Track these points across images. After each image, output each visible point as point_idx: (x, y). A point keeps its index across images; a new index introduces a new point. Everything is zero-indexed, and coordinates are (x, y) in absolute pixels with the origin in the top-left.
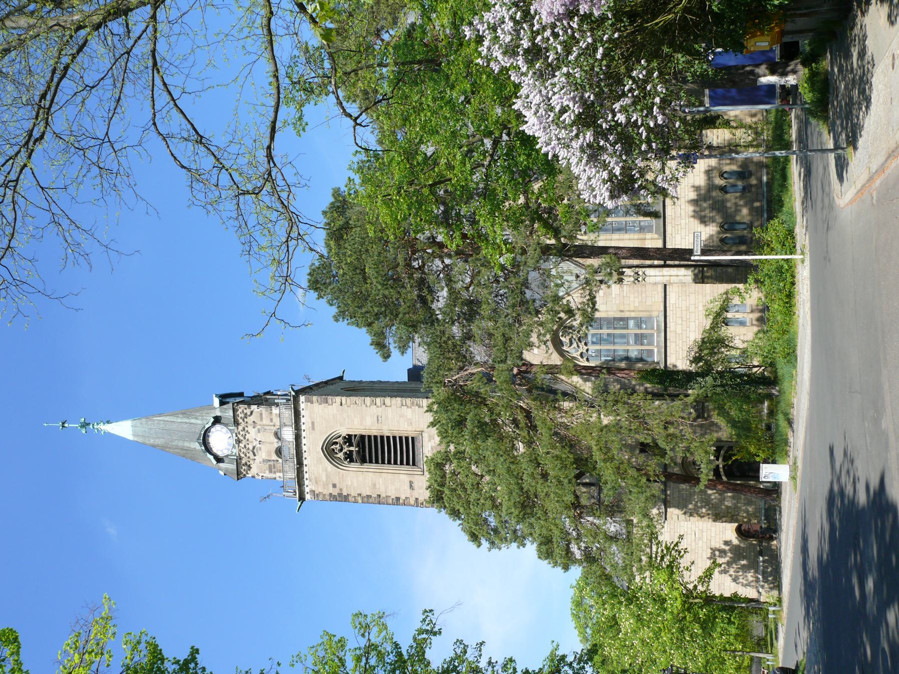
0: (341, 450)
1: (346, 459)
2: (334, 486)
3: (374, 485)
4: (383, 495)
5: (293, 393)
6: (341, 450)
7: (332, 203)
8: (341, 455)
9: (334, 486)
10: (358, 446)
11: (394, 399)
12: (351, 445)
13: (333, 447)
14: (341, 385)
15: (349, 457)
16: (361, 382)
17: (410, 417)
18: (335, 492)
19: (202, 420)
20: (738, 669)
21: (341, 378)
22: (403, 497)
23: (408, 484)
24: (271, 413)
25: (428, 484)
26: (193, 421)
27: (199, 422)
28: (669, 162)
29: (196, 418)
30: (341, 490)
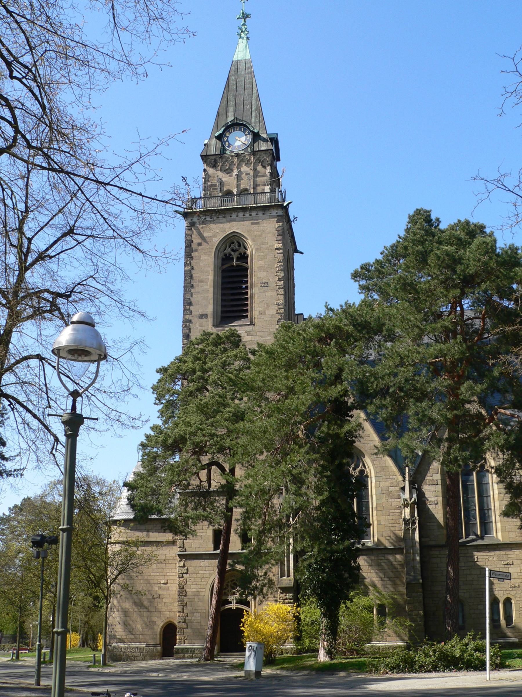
0: (233, 250)
1: (225, 255)
2: (199, 244)
3: (202, 281)
4: (193, 290)
5: (285, 204)
6: (233, 250)
7: (369, 264)
8: (228, 250)
9: (199, 244)
10: (238, 266)
11: (282, 297)
12: (238, 259)
13: (236, 244)
14: (291, 250)
15: (227, 258)
16: (293, 269)
17: (268, 312)
18: (194, 246)
19: (255, 122)
20: (3, 529)
21: (296, 251)
22: (192, 308)
23: (204, 313)
24: (265, 185)
25: (488, 231)
26: (254, 114)
27: (253, 120)
28: (236, 476)
29: (256, 117)
30: (196, 251)
